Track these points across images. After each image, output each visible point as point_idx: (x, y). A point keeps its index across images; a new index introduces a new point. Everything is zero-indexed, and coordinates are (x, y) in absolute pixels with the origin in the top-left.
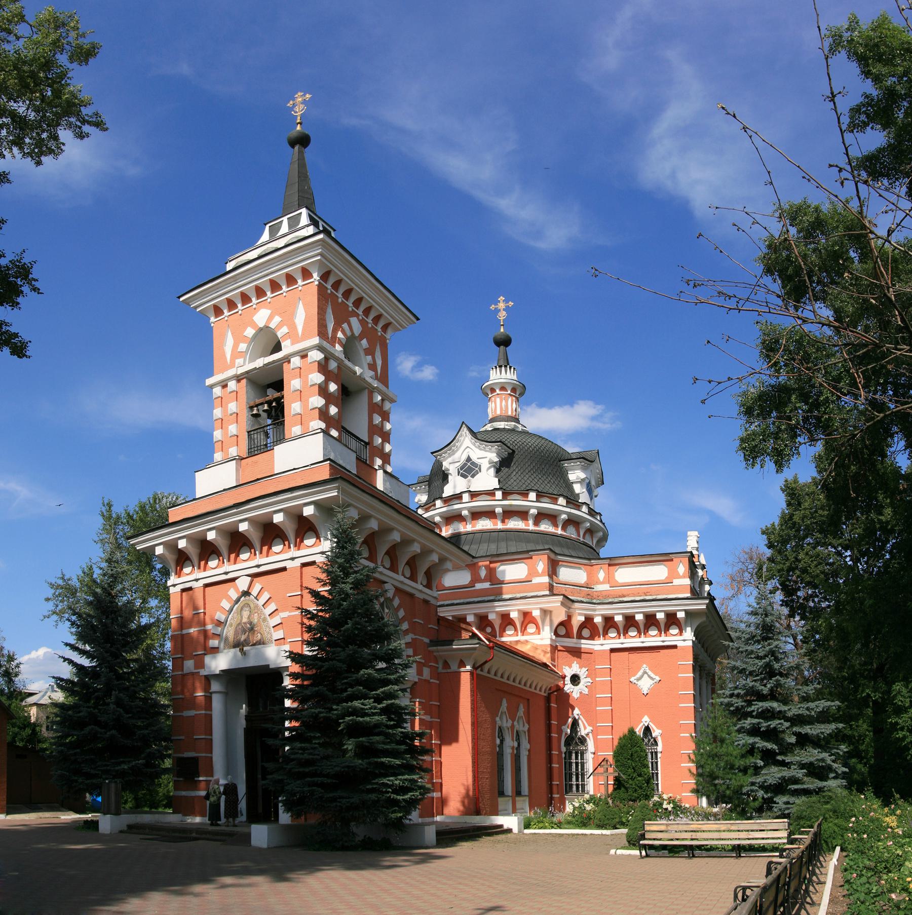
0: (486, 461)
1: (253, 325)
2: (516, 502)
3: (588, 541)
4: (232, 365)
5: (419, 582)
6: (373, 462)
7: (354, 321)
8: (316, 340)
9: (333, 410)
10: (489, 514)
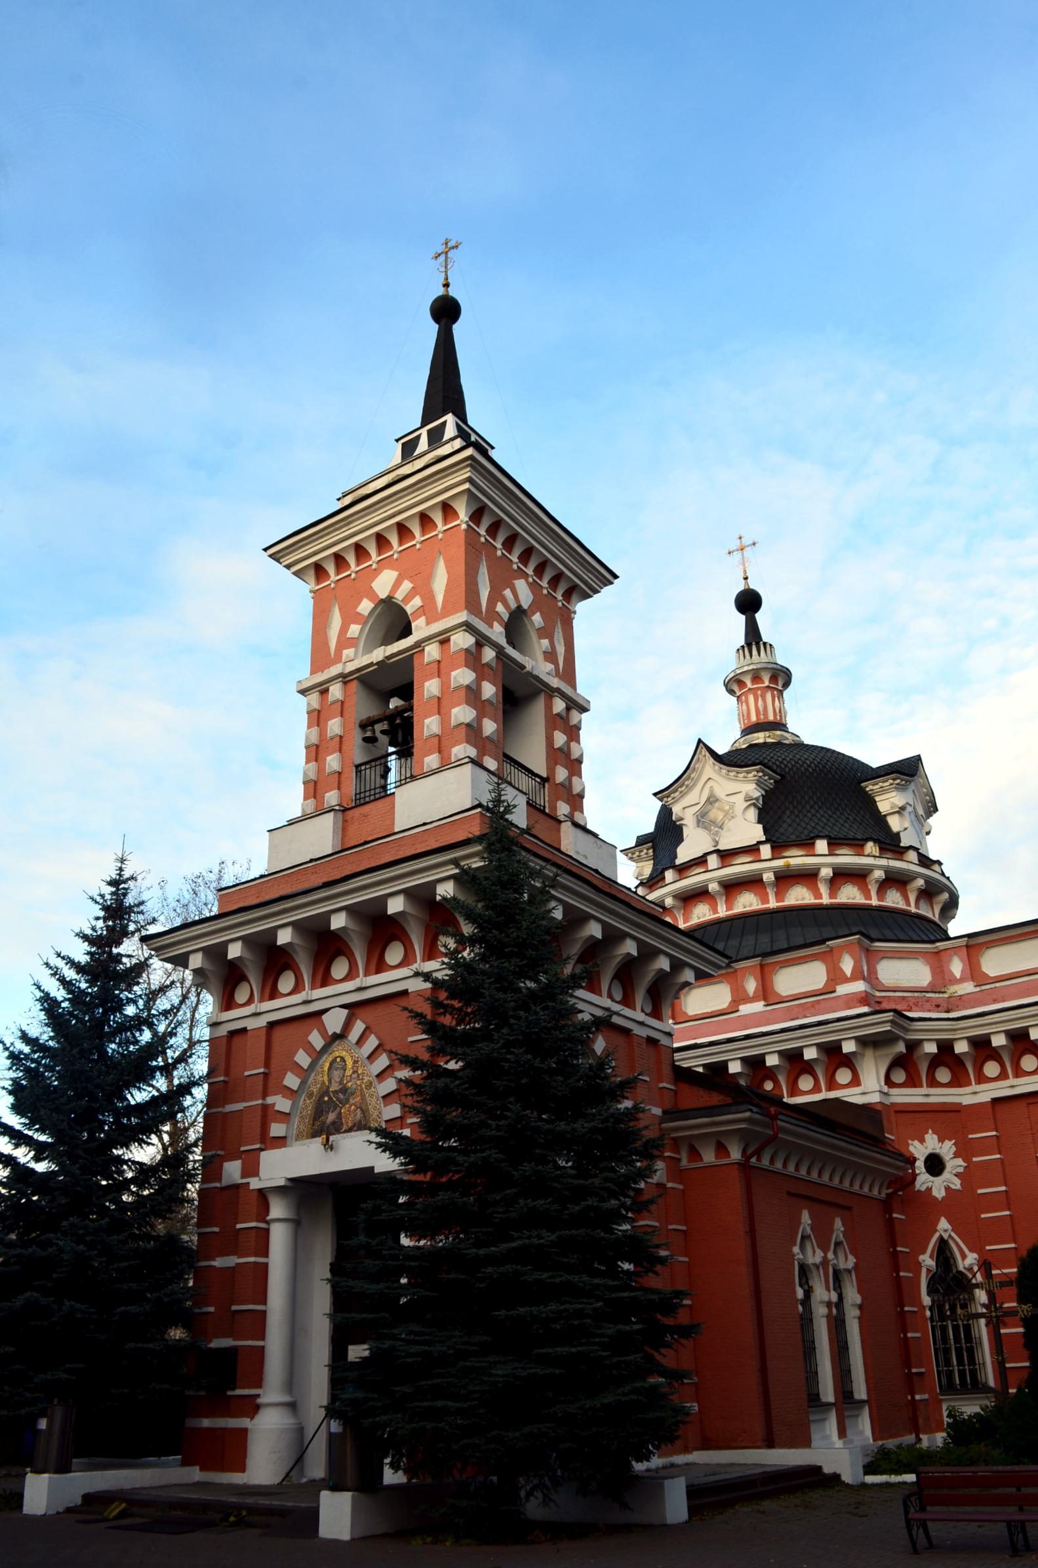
0: (741, 796)
1: (371, 594)
2: (796, 859)
3: (925, 911)
5: (638, 1007)
7: (521, 585)
8: (462, 616)
10: (752, 882)
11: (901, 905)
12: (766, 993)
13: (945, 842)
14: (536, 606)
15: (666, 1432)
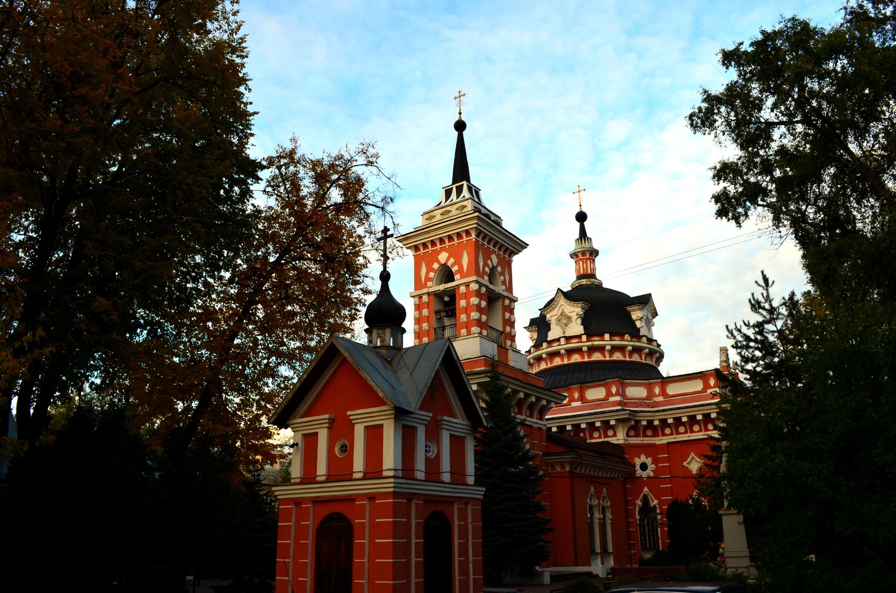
1: (438, 262)
3: (649, 362)
4: (425, 286)
6: (505, 343)
7: (494, 257)
8: (474, 278)
9: (484, 318)
11: (639, 360)
12: (582, 398)
13: (662, 331)
14: (498, 264)
15: (543, 559)
